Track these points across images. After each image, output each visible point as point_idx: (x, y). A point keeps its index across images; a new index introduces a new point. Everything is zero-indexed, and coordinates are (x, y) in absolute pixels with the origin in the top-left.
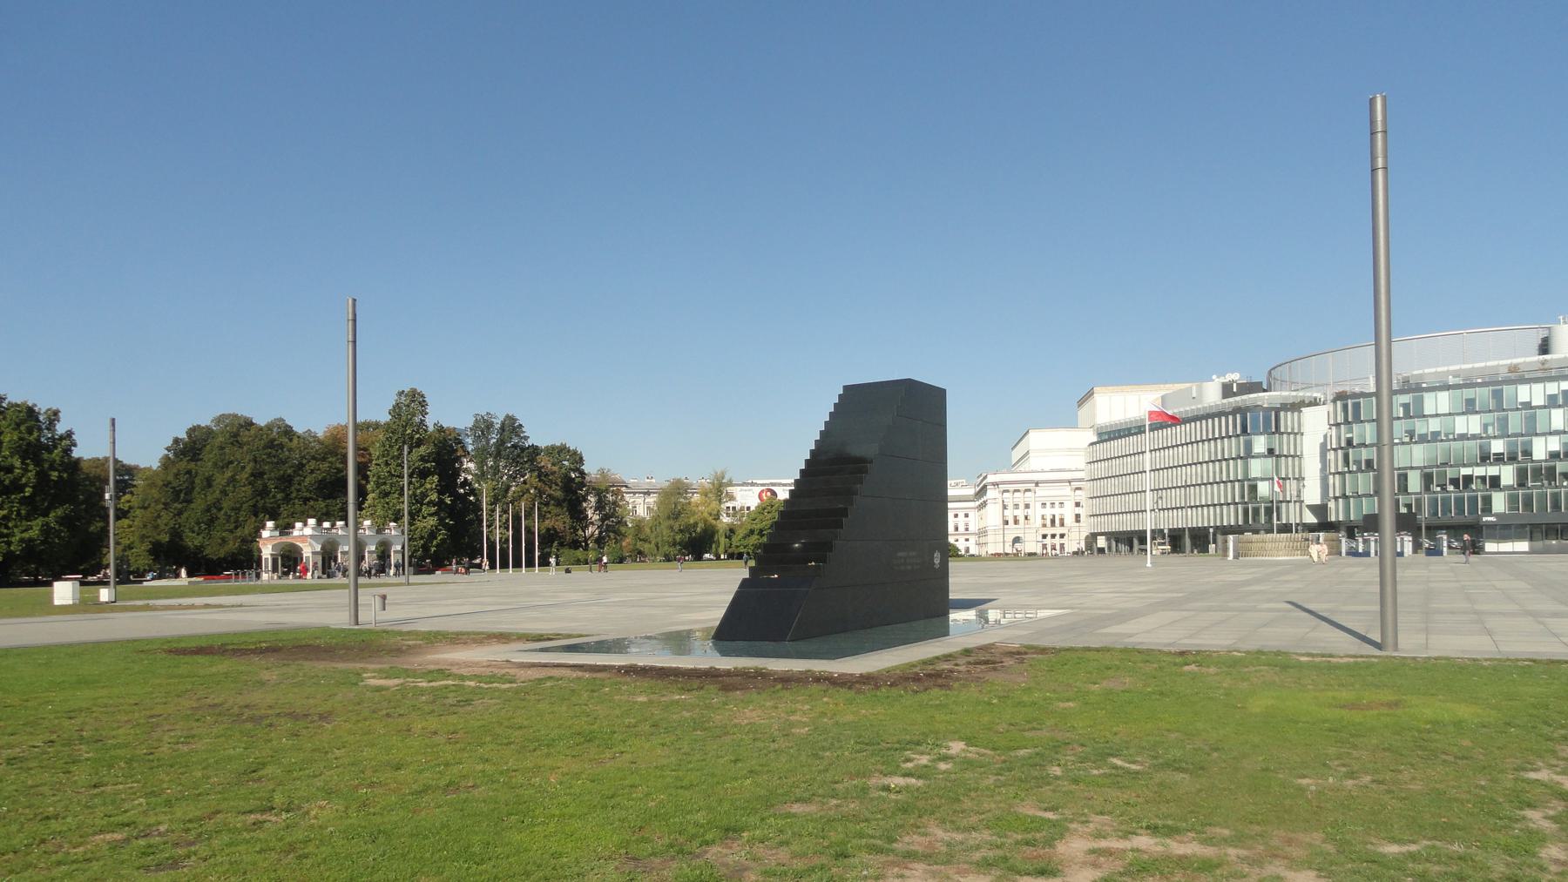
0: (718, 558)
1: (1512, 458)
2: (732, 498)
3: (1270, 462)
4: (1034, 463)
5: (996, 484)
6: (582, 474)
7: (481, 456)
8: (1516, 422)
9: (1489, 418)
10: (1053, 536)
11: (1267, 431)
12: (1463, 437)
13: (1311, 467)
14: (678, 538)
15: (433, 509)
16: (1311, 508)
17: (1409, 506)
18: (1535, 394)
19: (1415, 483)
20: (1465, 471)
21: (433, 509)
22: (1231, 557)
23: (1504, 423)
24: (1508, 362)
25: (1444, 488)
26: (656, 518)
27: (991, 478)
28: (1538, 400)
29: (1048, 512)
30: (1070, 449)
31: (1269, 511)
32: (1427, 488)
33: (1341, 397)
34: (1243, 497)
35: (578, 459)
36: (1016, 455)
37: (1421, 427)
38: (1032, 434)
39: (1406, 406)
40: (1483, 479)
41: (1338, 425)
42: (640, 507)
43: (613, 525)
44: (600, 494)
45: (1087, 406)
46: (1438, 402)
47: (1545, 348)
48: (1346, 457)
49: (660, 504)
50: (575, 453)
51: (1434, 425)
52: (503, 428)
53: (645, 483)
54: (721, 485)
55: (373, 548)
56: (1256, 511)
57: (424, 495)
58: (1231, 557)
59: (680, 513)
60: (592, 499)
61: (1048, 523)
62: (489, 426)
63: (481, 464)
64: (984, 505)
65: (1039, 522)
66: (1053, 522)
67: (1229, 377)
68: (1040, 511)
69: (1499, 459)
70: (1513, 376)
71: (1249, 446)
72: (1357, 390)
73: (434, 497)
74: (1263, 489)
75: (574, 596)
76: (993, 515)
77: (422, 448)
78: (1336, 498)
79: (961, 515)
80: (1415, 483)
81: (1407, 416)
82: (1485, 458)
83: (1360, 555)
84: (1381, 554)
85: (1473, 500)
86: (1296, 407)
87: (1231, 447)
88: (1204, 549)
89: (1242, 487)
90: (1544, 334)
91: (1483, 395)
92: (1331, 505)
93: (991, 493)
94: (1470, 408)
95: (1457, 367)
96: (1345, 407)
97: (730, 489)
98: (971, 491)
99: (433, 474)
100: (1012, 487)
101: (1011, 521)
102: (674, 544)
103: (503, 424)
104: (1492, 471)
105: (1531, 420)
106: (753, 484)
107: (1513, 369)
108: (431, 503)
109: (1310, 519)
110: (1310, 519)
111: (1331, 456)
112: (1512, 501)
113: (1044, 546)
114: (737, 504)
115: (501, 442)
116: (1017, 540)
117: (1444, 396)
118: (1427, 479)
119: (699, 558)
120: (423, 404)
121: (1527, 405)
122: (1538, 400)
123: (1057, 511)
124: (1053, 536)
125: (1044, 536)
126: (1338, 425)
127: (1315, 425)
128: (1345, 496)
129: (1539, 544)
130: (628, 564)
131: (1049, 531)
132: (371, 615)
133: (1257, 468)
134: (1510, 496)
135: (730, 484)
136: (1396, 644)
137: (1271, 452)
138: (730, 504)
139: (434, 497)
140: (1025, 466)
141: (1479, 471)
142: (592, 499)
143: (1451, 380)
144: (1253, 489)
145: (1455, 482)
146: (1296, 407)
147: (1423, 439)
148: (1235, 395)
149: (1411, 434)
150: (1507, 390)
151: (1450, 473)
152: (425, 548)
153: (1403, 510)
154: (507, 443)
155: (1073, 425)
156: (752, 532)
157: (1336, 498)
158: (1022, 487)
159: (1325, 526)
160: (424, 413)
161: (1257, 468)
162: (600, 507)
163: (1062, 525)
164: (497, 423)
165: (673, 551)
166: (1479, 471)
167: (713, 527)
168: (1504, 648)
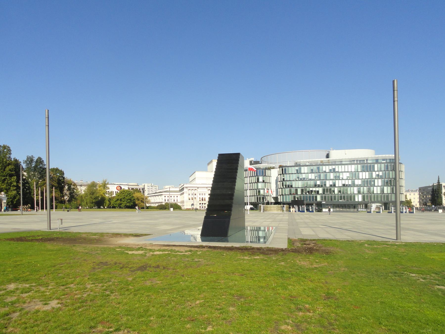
0: (104, 208)
1: (322, 186)
2: (109, 188)
3: (263, 184)
4: (197, 181)
5: (187, 187)
6: (64, 178)
7: (28, 170)
8: (322, 176)
9: (316, 175)
10: (203, 204)
11: (262, 175)
12: (311, 180)
13: (273, 186)
14: (94, 201)
15: (15, 188)
16: (273, 198)
17: (298, 198)
18: (326, 169)
19: (299, 192)
20: (311, 189)
21: (15, 188)
22: (262, 211)
23: (320, 176)
24: (320, 160)
25: (306, 193)
26: (86, 194)
27: (185, 186)
28: (327, 171)
29: (201, 196)
30: (207, 178)
31: (263, 198)
32: (302, 193)
33: (280, 167)
34: (256, 194)
35: (62, 173)
36: (191, 179)
37: (301, 176)
38: (197, 173)
39: (297, 170)
40: (315, 191)
41: (280, 174)
42: (82, 190)
43: (72, 197)
44: (69, 185)
45: (210, 165)
46: (305, 170)
47: (328, 156)
48: (283, 184)
49: (88, 189)
50: (61, 171)
51: (304, 176)
52: (37, 161)
53: (84, 182)
54: (105, 184)
55: (5, 201)
56: (260, 198)
57: (11, 183)
58: (262, 211)
59: (94, 193)
60: (66, 187)
61: (201, 200)
62: (32, 160)
63: (28, 173)
64: (183, 193)
65: (199, 199)
66: (202, 199)
67: (251, 159)
68: (199, 196)
69: (319, 186)
70: (321, 163)
71: (258, 179)
72: (285, 165)
73: (15, 184)
74: (262, 192)
75: (380, 228)
76: (186, 197)
77: (10, 166)
78: (280, 195)
79: (176, 196)
80: (299, 192)
81: (297, 173)
82: (315, 186)
83: (310, 212)
84: (396, 212)
85: (313, 197)
86: (269, 169)
87: (254, 179)
88: (320, 211)
89: (256, 191)
90: (328, 153)
91: (315, 168)
92: (279, 197)
93: (185, 190)
94: (312, 172)
95: (308, 160)
96: (282, 169)
97: (108, 186)
98: (178, 189)
99: (14, 176)
100: (191, 189)
101: (191, 199)
102: (93, 203)
103: (37, 159)
104: (317, 189)
105: (326, 176)
106: (115, 184)
107: (322, 162)
108: (14, 186)
109: (273, 201)
110: (273, 201)
111: (279, 183)
112: (322, 198)
113: (200, 207)
114: (110, 190)
115: (36, 166)
116: (193, 205)
117: (306, 168)
118: (302, 191)
119: (99, 207)
120: (9, 150)
121: (325, 172)
122: (327, 171)
123: (204, 196)
124: (203, 204)
125: (200, 204)
126: (280, 174)
127: (274, 174)
128: (282, 195)
129: (335, 209)
130: (117, 209)
131: (201, 202)
132: (56, 226)
133: (260, 186)
134: (321, 196)
135: (108, 184)
136: (400, 239)
137: (264, 181)
138: (108, 190)
139: (15, 184)
140: (194, 182)
141: (314, 189)
142: (66, 187)
143: (307, 164)
144: (259, 192)
145: (309, 192)
146: (269, 169)
147: (301, 180)
148: (253, 164)
149: (298, 178)
150: (321, 167)
151: (308, 189)
152: (12, 202)
153: (296, 199)
154: (38, 167)
155: (206, 170)
156: (118, 200)
157: (280, 195)
158: (194, 189)
159: (277, 203)
160: (10, 154)
161: (260, 186)
162: (69, 189)
163: (205, 200)
164: (35, 159)
165: (92, 205)
166: (314, 189)
167: (104, 197)
168: (337, 237)
